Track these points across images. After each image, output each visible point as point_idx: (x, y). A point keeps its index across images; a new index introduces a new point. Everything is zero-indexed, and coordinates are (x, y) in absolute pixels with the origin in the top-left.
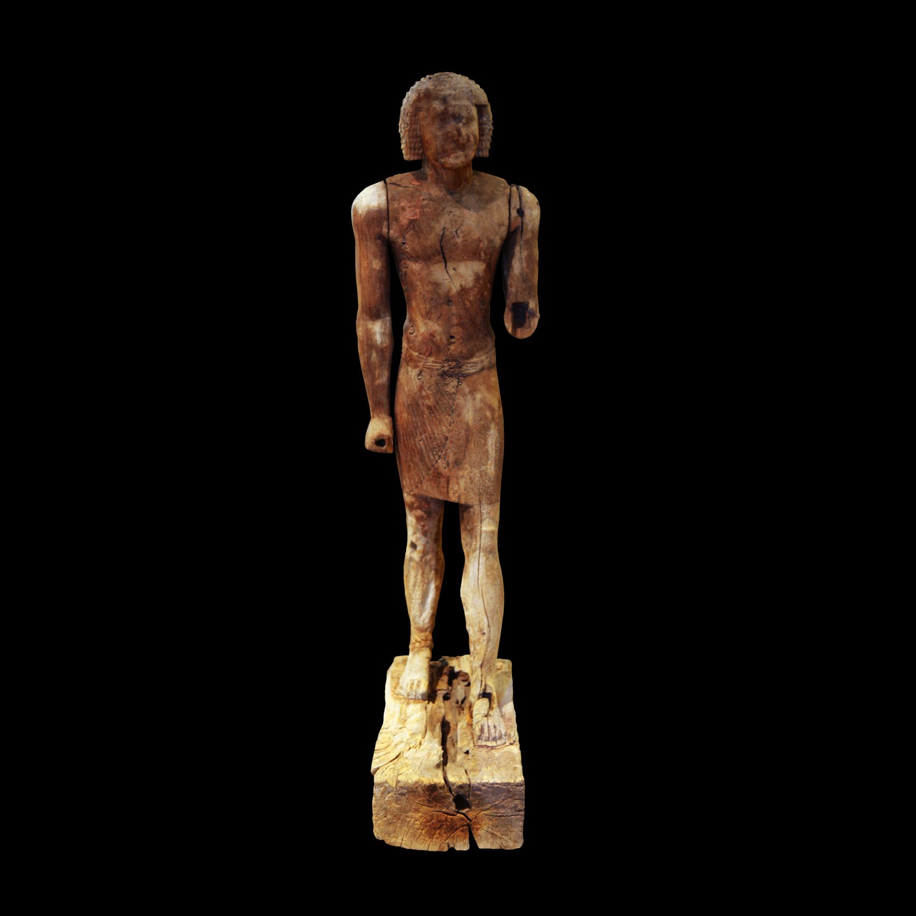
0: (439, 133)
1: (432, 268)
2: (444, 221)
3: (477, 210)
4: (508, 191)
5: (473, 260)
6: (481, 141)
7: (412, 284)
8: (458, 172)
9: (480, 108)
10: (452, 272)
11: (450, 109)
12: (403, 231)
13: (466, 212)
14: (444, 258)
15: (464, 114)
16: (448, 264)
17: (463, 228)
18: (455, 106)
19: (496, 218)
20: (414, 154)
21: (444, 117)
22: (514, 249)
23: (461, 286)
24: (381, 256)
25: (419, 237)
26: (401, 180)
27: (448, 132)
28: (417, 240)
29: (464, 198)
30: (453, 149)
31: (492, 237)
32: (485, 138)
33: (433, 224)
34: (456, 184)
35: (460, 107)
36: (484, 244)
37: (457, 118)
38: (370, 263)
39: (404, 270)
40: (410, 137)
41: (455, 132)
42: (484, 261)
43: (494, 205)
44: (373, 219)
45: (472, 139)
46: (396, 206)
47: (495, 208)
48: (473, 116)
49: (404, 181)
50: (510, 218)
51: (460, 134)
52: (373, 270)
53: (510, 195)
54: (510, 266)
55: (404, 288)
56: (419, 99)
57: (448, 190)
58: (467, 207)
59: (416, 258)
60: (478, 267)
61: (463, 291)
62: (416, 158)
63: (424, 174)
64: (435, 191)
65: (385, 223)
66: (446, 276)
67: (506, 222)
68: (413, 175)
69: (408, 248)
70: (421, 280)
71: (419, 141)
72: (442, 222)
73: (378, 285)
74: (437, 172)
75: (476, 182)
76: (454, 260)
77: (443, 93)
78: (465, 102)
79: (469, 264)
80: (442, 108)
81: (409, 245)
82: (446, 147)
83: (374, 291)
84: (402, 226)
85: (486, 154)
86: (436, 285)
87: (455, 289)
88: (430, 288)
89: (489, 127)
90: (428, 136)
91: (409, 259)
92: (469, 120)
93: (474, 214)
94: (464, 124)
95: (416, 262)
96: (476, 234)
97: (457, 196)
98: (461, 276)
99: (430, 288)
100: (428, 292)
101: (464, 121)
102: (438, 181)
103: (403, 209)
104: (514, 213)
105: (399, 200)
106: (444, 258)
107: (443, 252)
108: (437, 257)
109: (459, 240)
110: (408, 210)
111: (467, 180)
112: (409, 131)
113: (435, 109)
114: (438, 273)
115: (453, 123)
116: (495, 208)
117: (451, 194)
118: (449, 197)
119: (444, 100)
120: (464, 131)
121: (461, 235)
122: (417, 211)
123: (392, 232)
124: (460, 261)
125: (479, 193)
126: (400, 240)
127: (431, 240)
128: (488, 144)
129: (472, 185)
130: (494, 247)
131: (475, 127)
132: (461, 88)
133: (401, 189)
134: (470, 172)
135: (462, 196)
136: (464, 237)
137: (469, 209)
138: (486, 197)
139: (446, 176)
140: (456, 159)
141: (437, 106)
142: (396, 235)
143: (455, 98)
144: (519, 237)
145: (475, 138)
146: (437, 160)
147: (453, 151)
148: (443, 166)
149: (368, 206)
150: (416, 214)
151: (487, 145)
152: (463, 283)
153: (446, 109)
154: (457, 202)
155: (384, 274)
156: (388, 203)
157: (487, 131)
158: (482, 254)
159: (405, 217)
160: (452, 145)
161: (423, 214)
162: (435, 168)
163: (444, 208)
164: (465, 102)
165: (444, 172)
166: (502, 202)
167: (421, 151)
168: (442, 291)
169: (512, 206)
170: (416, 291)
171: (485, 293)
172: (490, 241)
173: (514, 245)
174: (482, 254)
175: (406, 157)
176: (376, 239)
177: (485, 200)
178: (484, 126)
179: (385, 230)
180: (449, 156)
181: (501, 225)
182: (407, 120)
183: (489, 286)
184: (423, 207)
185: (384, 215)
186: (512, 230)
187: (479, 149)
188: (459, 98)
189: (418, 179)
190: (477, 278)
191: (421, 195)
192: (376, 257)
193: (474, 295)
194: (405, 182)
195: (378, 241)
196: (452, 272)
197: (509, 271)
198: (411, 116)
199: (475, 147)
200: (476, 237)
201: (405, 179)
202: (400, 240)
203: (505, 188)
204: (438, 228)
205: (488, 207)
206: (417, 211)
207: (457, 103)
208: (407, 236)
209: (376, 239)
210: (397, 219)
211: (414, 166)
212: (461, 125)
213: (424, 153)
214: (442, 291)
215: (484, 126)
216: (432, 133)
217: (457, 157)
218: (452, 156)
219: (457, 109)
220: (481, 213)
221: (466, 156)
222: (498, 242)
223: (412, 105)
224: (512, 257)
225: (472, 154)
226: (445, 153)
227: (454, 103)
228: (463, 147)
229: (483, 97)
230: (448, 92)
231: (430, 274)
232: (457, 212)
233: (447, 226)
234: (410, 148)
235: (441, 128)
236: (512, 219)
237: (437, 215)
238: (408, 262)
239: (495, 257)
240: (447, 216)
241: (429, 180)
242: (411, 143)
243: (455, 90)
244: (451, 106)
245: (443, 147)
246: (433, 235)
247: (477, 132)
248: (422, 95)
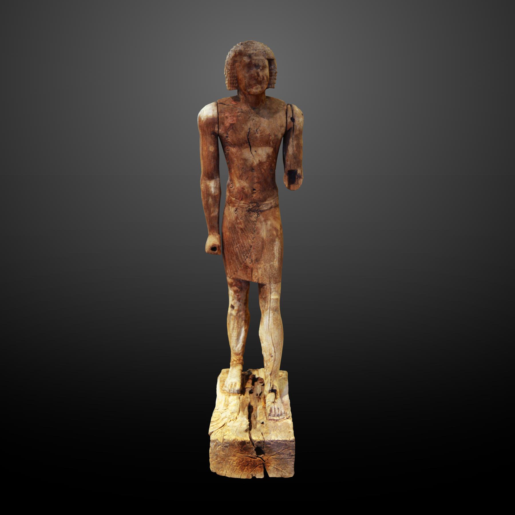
0: (247, 75)
1: (243, 151)
2: (250, 124)
3: (268, 118)
5: (266, 146)
6: (270, 79)
10: (254, 153)
11: (253, 61)
12: (227, 130)
13: (262, 119)
14: (250, 145)
15: (261, 64)
16: (252, 149)
17: (260, 128)
18: (256, 59)
19: (279, 122)
21: (250, 66)
22: (289, 140)
23: (259, 161)
24: (214, 144)
25: (236, 133)
27: (252, 74)
28: (234, 135)
29: (261, 112)
30: (255, 84)
31: (277, 133)
33: (243, 126)
35: (259, 60)
36: (272, 137)
37: (257, 66)
38: (208, 148)
40: (230, 77)
41: (256, 74)
42: (272, 147)
43: (278, 115)
44: (210, 123)
45: (265, 78)
46: (223, 116)
47: (278, 117)
48: (266, 65)
50: (286, 123)
51: (258, 75)
52: (209, 152)
53: (287, 110)
56: (235, 56)
57: (252, 107)
58: (263, 117)
59: (234, 145)
61: (261, 163)
64: (245, 108)
65: (217, 126)
66: (251, 155)
67: (285, 125)
69: (229, 139)
70: (237, 157)
72: (249, 125)
73: (213, 160)
74: (246, 97)
76: (255, 146)
77: (249, 52)
78: (262, 58)
79: (264, 148)
80: (249, 61)
82: (251, 83)
83: (211, 164)
84: (226, 127)
86: (245, 160)
87: (256, 162)
88: (242, 162)
90: (240, 77)
91: (230, 146)
92: (264, 67)
93: (267, 120)
94: (261, 70)
95: (234, 147)
96: (268, 132)
97: (257, 110)
98: (259, 155)
99: (242, 162)
100: (241, 164)
101: (261, 68)
102: (246, 102)
103: (227, 117)
104: (289, 120)
105: (224, 113)
106: (250, 145)
107: (249, 142)
108: (246, 145)
109: (258, 135)
110: (229, 118)
111: (262, 101)
112: (230, 73)
113: (244, 61)
114: (246, 153)
115: (255, 69)
116: (278, 117)
117: (254, 109)
118: (252, 111)
119: (250, 56)
120: (261, 74)
121: (259, 132)
122: (235, 118)
123: (220, 130)
124: (258, 147)
125: (270, 109)
126: (225, 135)
127: (243, 135)
129: (266, 104)
131: (267, 71)
133: (225, 106)
135: (260, 110)
136: (261, 133)
137: (264, 118)
138: (273, 111)
139: (251, 99)
141: (246, 59)
142: (223, 132)
143: (256, 55)
144: (292, 133)
145: (267, 77)
146: (246, 90)
147: (255, 85)
148: (249, 93)
149: (207, 116)
150: (234, 120)
152: (260, 159)
153: (251, 61)
154: (257, 113)
156: (218, 114)
158: (271, 143)
159: (228, 122)
160: (254, 82)
161: (238, 120)
163: (249, 117)
164: (262, 58)
165: (249, 96)
167: (237, 85)
168: (249, 164)
169: (288, 116)
170: (234, 163)
172: (275, 136)
174: (271, 143)
176: (211, 134)
178: (272, 71)
179: (216, 129)
180: (252, 88)
181: (281, 126)
184: (238, 116)
185: (216, 121)
186: (288, 129)
188: (258, 55)
191: (237, 110)
192: (211, 145)
193: (267, 166)
195: (213, 136)
196: (254, 153)
198: (231, 65)
199: (267, 83)
200: (268, 133)
202: (225, 135)
204: (246, 128)
205: (275, 116)
206: (235, 118)
207: (257, 58)
208: (229, 133)
209: (211, 134)
210: (223, 123)
212: (259, 70)
214: (249, 164)
215: (272, 71)
217: (257, 88)
218: (254, 88)
219: (257, 62)
220: (270, 120)
221: (262, 88)
223: (232, 59)
226: (250, 86)
227: (255, 58)
230: (252, 52)
231: (242, 154)
232: (257, 119)
233: (251, 127)
235: (248, 72)
236: (288, 123)
237: (246, 121)
238: (230, 147)
240: (251, 121)
241: (241, 101)
242: (231, 80)
243: (256, 50)
244: (254, 59)
245: (249, 82)
246: (243, 132)
247: (268, 74)
248: (237, 53)
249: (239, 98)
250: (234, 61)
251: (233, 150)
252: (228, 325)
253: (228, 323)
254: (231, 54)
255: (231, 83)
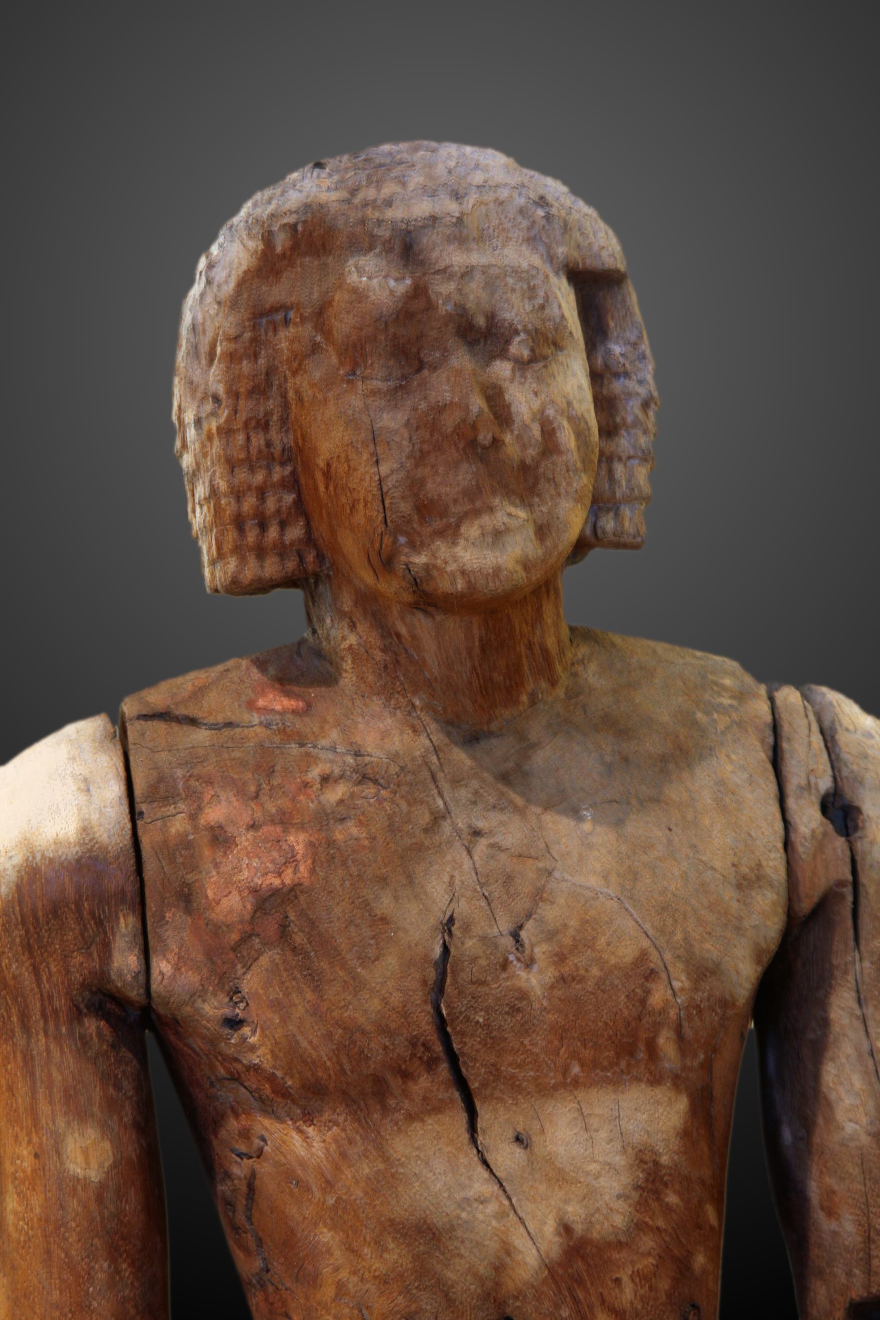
0: (392, 420)
1: (399, 1147)
2: (446, 883)
3: (616, 810)
4: (763, 708)
5: (616, 1083)
6: (607, 459)
7: (289, 1242)
9: (593, 286)
10: (507, 1157)
11: (443, 290)
12: (224, 956)
13: (561, 829)
14: (461, 1084)
15: (516, 311)
16: (485, 1116)
17: (551, 913)
18: (468, 273)
19: (719, 844)
21: (409, 340)
22: (823, 1005)
23: (566, 1229)
24: (111, 1105)
25: (316, 981)
26: (200, 692)
27: (440, 409)
28: (302, 1002)
29: (539, 759)
30: (472, 494)
31: (710, 949)
32: (624, 443)
33: (385, 904)
35: (493, 280)
36: (671, 992)
37: (484, 335)
38: (48, 1154)
39: (239, 1170)
40: (231, 465)
41: (477, 403)
42: (678, 1082)
43: (700, 783)
44: (55, 910)
45: (567, 437)
46: (178, 825)
47: (707, 798)
48: (560, 324)
49: (212, 699)
50: (787, 844)
51: (501, 413)
52: (70, 1185)
53: (775, 727)
55: (247, 1266)
56: (269, 265)
57: (450, 723)
58: (565, 803)
59: (306, 1095)
60: (649, 1116)
61: (580, 1257)
64: (381, 732)
65: (126, 925)
66: (480, 1184)
67: (774, 864)
69: (257, 1045)
70: (342, 1216)
72: (437, 889)
73: (102, 1268)
74: (387, 632)
75: (592, 675)
76: (515, 1087)
77: (396, 213)
78: (518, 255)
79: (601, 1102)
80: (403, 287)
81: (263, 1022)
82: (433, 488)
83: (118, 1272)
84: (217, 930)
86: (427, 1236)
87: (533, 1249)
88: (396, 1255)
90: (329, 442)
91: (267, 1108)
92: (546, 344)
93: (602, 836)
94: (522, 365)
95: (309, 1117)
96: (625, 939)
97: (501, 747)
98: (559, 1177)
99: (396, 1255)
100: (383, 1281)
101: (519, 347)
102: (398, 673)
103: (220, 838)
104: (809, 818)
105: (192, 795)
106: (461, 1084)
107: (448, 1055)
108: (423, 1083)
109: (535, 980)
110: (245, 840)
111: (546, 666)
112: (226, 432)
113: (358, 295)
114: (434, 1166)
115: (461, 359)
116: (707, 798)
117: (471, 739)
118: (460, 757)
119: (407, 248)
120: (523, 401)
121: (541, 951)
122: (298, 841)
123: (162, 966)
124: (545, 1091)
125: (616, 726)
126: (213, 1008)
127: (384, 990)
129: (573, 694)
130: (725, 1004)
131: (572, 378)
133: (201, 736)
135: (528, 748)
136: (560, 958)
137: (575, 813)
138: (652, 745)
139: (435, 641)
141: (373, 280)
142: (190, 979)
143: (460, 232)
144: (842, 953)
145: (581, 435)
146: (386, 563)
147: (475, 503)
148: (426, 598)
149: (27, 843)
150: (291, 860)
152: (575, 1212)
153: (419, 292)
154: (504, 778)
156: (134, 814)
157: (632, 410)
158: (666, 1042)
159: (231, 885)
160: (466, 475)
161: (327, 854)
162: (370, 605)
163: (437, 818)
164: (518, 255)
165: (423, 626)
166: (736, 767)
167: (295, 532)
168: (462, 1271)
169: (795, 778)
170: (314, 1281)
171: (700, 1260)
172: (703, 972)
173: (823, 982)
174: (666, 1042)
176: (77, 1014)
177: (649, 764)
178: (617, 386)
179: (125, 961)
180: (451, 532)
181: (748, 882)
182: (214, 378)
183: (711, 1214)
184: (325, 819)
185: (119, 878)
186: (806, 906)
188: (482, 238)
190: (651, 1178)
191: (309, 760)
192: (81, 1115)
193: (640, 1277)
194: (218, 704)
195: (92, 1025)
196: (507, 1157)
197: (806, 1125)
198: (232, 357)
199: (584, 481)
200: (627, 953)
202: (213, 1008)
203: (741, 696)
204: (415, 925)
205: (674, 792)
206: (298, 841)
207: (476, 258)
208: (251, 982)
209: (77, 1014)
210: (187, 897)
212: (502, 369)
213: (309, 539)
214: (462, 1271)
215: (617, 386)
216: (360, 431)
217: (498, 535)
218: (471, 530)
219: (475, 294)
220: (640, 826)
221: (542, 531)
222: (743, 973)
223: (234, 303)
224: (819, 1049)
226: (432, 516)
227: (457, 258)
228: (527, 482)
230: (422, 208)
231: (387, 1180)
232: (511, 832)
233: (462, 908)
235: (399, 391)
236: (803, 848)
237: (406, 854)
238: (264, 1125)
240: (458, 853)
241: (348, 679)
242: (238, 495)
243: (457, 196)
244: (445, 272)
245: (414, 486)
246: (391, 961)
247: (586, 407)
248: (281, 242)
249: (319, 654)
250: (259, 312)
251: (299, 1145)
254: (229, 254)
255: (239, 523)
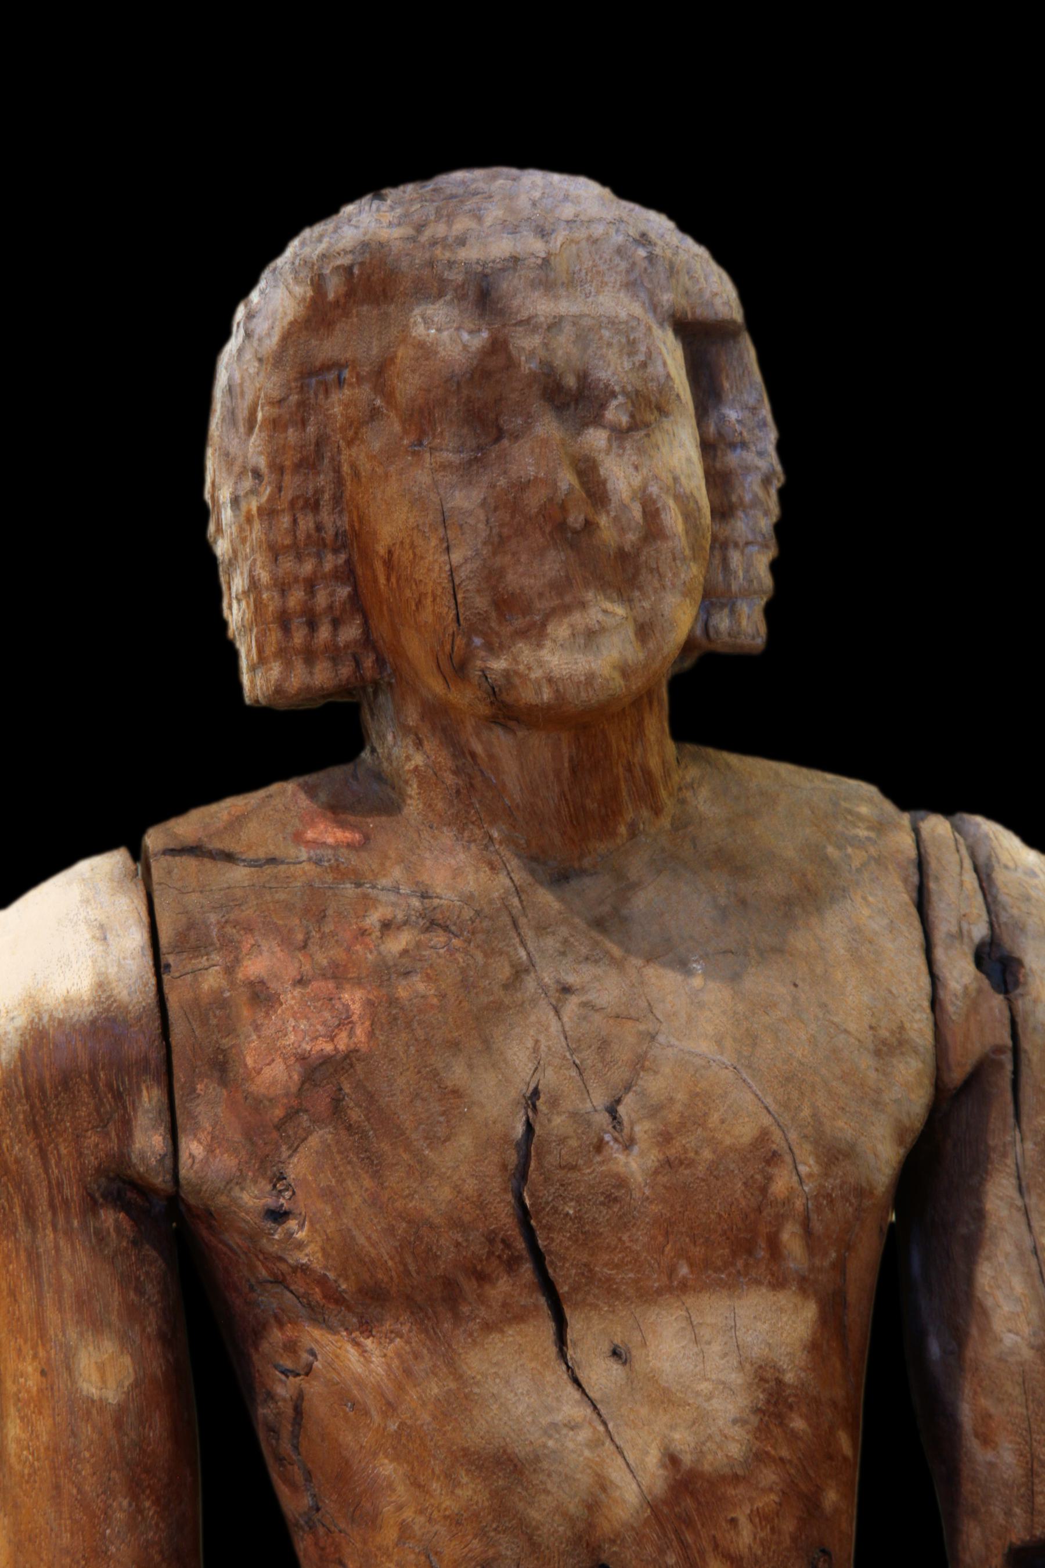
0: (465, 499)
1: (474, 1362)
2: (530, 1049)
3: (732, 963)
4: (906, 841)
5: (731, 1286)
6: (721, 545)
7: (343, 1475)
8: (584, 727)
9: (697, 335)
10: (602, 1374)
11: (526, 345)
12: (266, 1136)
13: (666, 985)
14: (548, 1287)
15: (612, 369)
16: (576, 1326)
17: (654, 1085)
18: (555, 324)
19: (854, 1003)
20: (309, 656)
21: (485, 403)
22: (977, 1193)
23: (672, 1460)
24: (132, 1313)
25: (375, 1165)
27: (523, 486)
28: (358, 1190)
29: (641, 901)
30: (561, 586)
31: (843, 1128)
32: (740, 527)
33: (457, 1074)
34: (576, 808)
35: (585, 332)
36: (796, 1179)
37: (575, 398)
38: (57, 1370)
39: (284, 1389)
40: (275, 552)
41: (567, 479)
42: (805, 1285)
43: (832, 930)
44: (66, 1081)
45: (673, 520)
46: (212, 980)
47: (839, 947)
48: (666, 385)
49: (252, 830)
50: (935, 1003)
51: (595, 491)
52: (83, 1408)
53: (921, 864)
54: (961, 1308)
55: (293, 1504)
56: (319, 315)
57: (535, 859)
58: (670, 954)
59: (363, 1301)
60: (768, 1327)
61: (689, 1494)
62: (323, 676)
63: (379, 776)
64: (454, 870)
65: (149, 1098)
66: (570, 1407)
67: (919, 1026)
68: (311, 792)
69: (305, 1242)
70: (406, 1444)
71: (339, 558)
72: (519, 1057)
73: (121, 1506)
74: (459, 751)
75: (703, 802)
76: (612, 1291)
77: (470, 254)
78: (615, 303)
79: (713, 1309)
80: (478, 341)
81: (310, 1214)
82: (514, 580)
83: (140, 1511)
84: (257, 1105)
85: (747, 626)
86: (507, 1469)
87: (632, 1483)
88: (470, 1491)
89: (760, 457)
90: (391, 525)
91: (317, 1316)
92: (648, 408)
93: (715, 994)
94: (620, 434)
95: (366, 1327)
96: (742, 1116)
97: (595, 888)
98: (664, 1398)
99: (470, 1491)
100: (455, 1521)
101: (616, 413)
102: (472, 799)
103: (261, 995)
104: (960, 972)
105: (229, 945)
106: (548, 1287)
107: (532, 1253)
108: (502, 1287)
109: (635, 1164)
110: (291, 997)
111: (648, 792)
112: (268, 513)
113: (426, 350)
114: (516, 1385)
115: (548, 427)
116: (839, 947)
117: (560, 878)
118: (547, 899)
119: (483, 294)
120: (620, 476)
121: (642, 1130)
122: (354, 999)
123: (192, 1148)
124: (647, 1296)
125: (732, 863)
126: (253, 1198)
127: (456, 1176)
128: (762, 561)
129: (680, 825)
130: (862, 1192)
131: (680, 449)
132: (580, 257)
133: (239, 874)
134: (657, 743)
135: (627, 888)
136: (665, 1138)
137: (683, 965)
138: (775, 885)
139: (516, 762)
140: (591, 650)
141: (443, 332)
142: (226, 1163)
143: (546, 276)
144: (1000, 1132)
145: (690, 516)
146: (458, 669)
147: (564, 598)
148: (505, 711)
149: (32, 1002)
150: (345, 1021)
151: (755, 566)
152: (682, 1439)
153: (497, 346)
154: (599, 924)
155: (157, 1430)
156: (159, 967)
158: (790, 1237)
159: (274, 1051)
160: (553, 564)
161: (388, 1014)
162: (440, 719)
163: (519, 972)
164: (615, 303)
165: (502, 743)
167: (350, 632)
168: (548, 1510)
169: (944, 924)
170: (372, 1521)
171: (831, 1497)
172: (835, 1154)
173: (977, 1167)
174: (790, 1237)
175: (256, 683)
176: (91, 1205)
177: (772, 910)
178: (733, 459)
179: (148, 1141)
180: (535, 632)
181: (888, 1048)
182: (254, 449)
183: (845, 1444)
184: (386, 973)
185: (142, 1043)
186: (957, 1076)
187: (713, 598)
188: (572, 282)
189: (337, 809)
190: (773, 1399)
191: (367, 902)
192: (96, 1325)
193: (760, 1517)
195: (109, 1218)
196: (602, 1374)
197: (958, 1337)
198: (275, 425)
199: (693, 572)
200: (745, 1132)
201: (272, 821)
202: (253, 1198)
203: (880, 827)
204: (493, 1099)
205: (800, 941)
206: (354, 999)
207: (565, 307)
208: (298, 1167)
209: (91, 1205)
210: (221, 1066)
211: (318, 740)
212: (596, 438)
213: (368, 641)
214: (548, 1510)
215: (733, 459)
216: (427, 512)
217: (591, 636)
218: (560, 630)
219: (564, 349)
220: (760, 981)
221: (644, 631)
222: (882, 1156)
223: (277, 360)
224: (973, 1247)
225: (681, 618)
226: (513, 613)
227: (543, 307)
228: (625, 572)
229: (718, 292)
230: (501, 247)
231: (460, 1402)
232: (607, 989)
233: (549, 1079)
234: (284, 621)
235: (474, 464)
236: (954, 1007)
237: (482, 1015)
238: (314, 1336)
239: (867, 1250)
240: (544, 1013)
241: (413, 807)
242: (283, 588)
243: (543, 233)
244: (529, 323)
245: (492, 577)
246: (465, 1142)
247: (696, 483)
248: (334, 288)
251: (355, 1360)
252: (871, 1312)
253: (868, 1342)
